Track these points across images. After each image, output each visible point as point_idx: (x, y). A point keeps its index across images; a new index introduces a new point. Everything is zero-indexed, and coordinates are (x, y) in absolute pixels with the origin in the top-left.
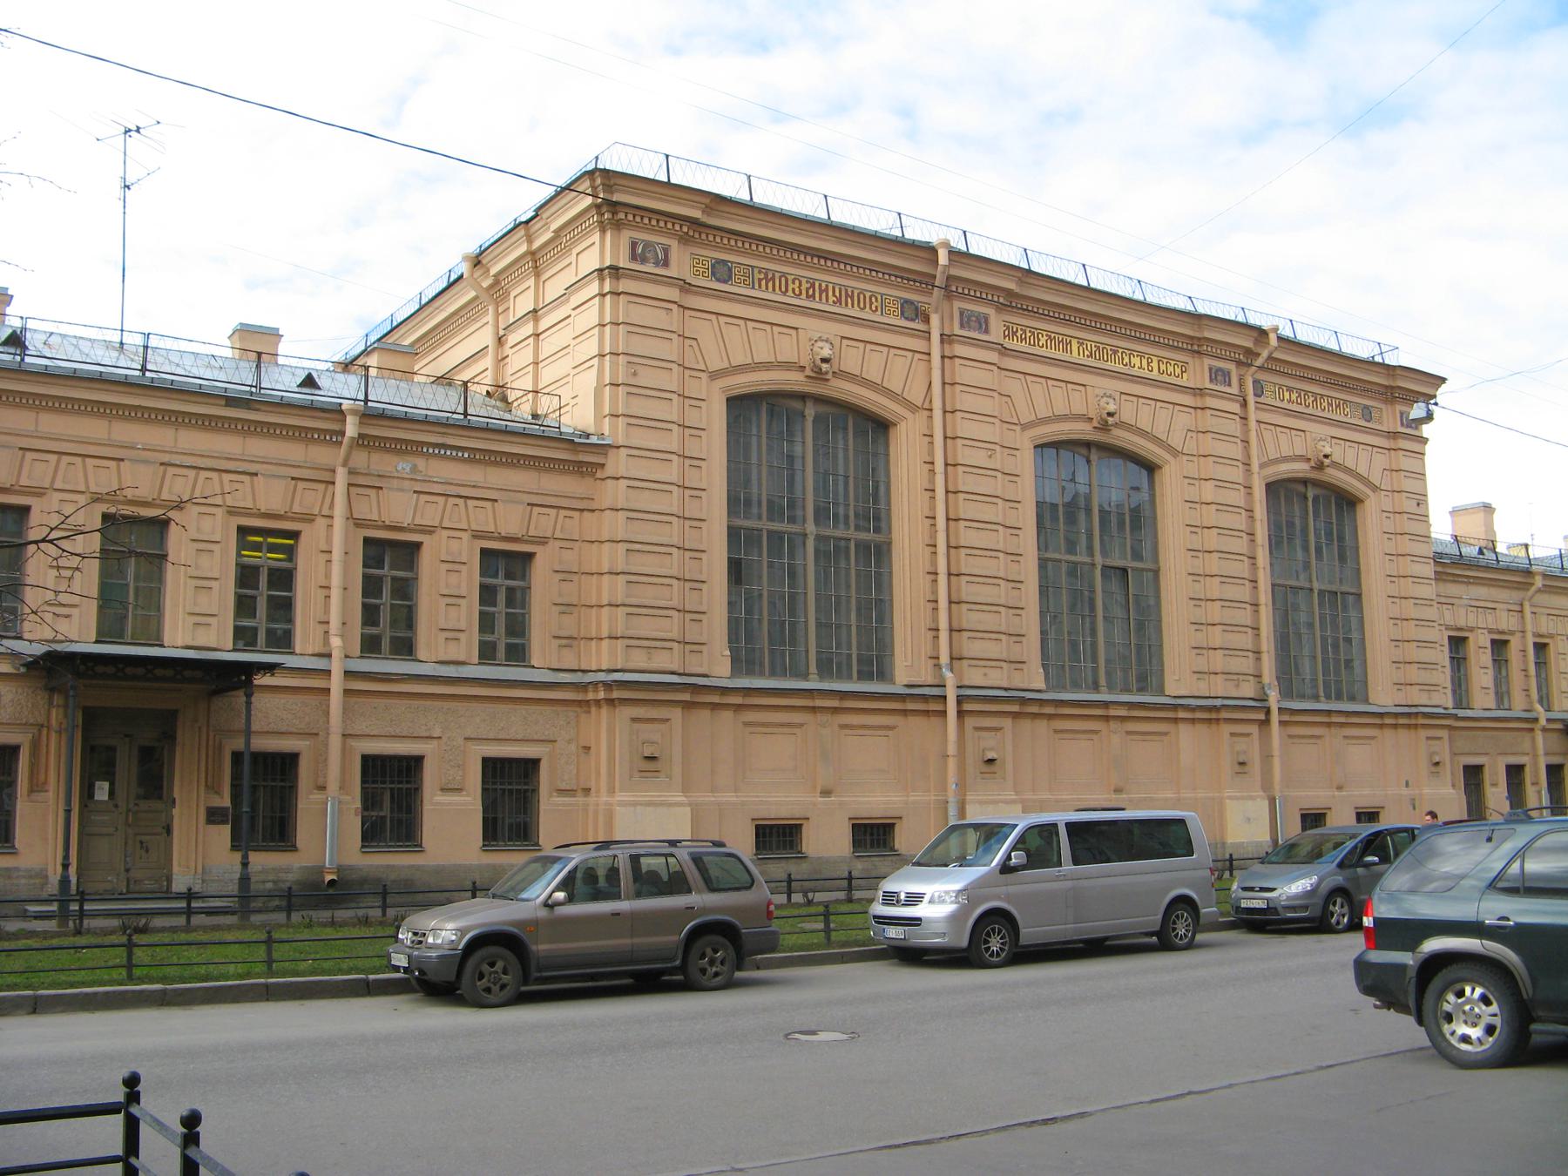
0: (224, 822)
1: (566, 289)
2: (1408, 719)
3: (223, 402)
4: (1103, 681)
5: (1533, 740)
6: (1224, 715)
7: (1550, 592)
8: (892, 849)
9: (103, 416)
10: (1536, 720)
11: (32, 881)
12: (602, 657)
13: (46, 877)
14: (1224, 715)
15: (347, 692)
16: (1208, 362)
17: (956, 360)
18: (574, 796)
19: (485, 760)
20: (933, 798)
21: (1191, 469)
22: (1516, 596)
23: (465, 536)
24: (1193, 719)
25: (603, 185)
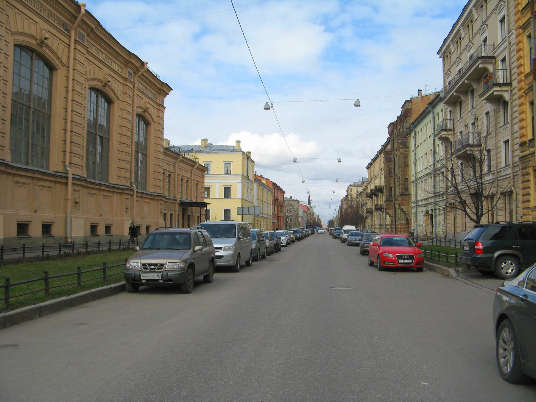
4: (30, 162)
5: (175, 206)
6: (126, 192)
8: (50, 235)
10: (176, 200)
14: (126, 192)
16: (129, 70)
20: (62, 215)
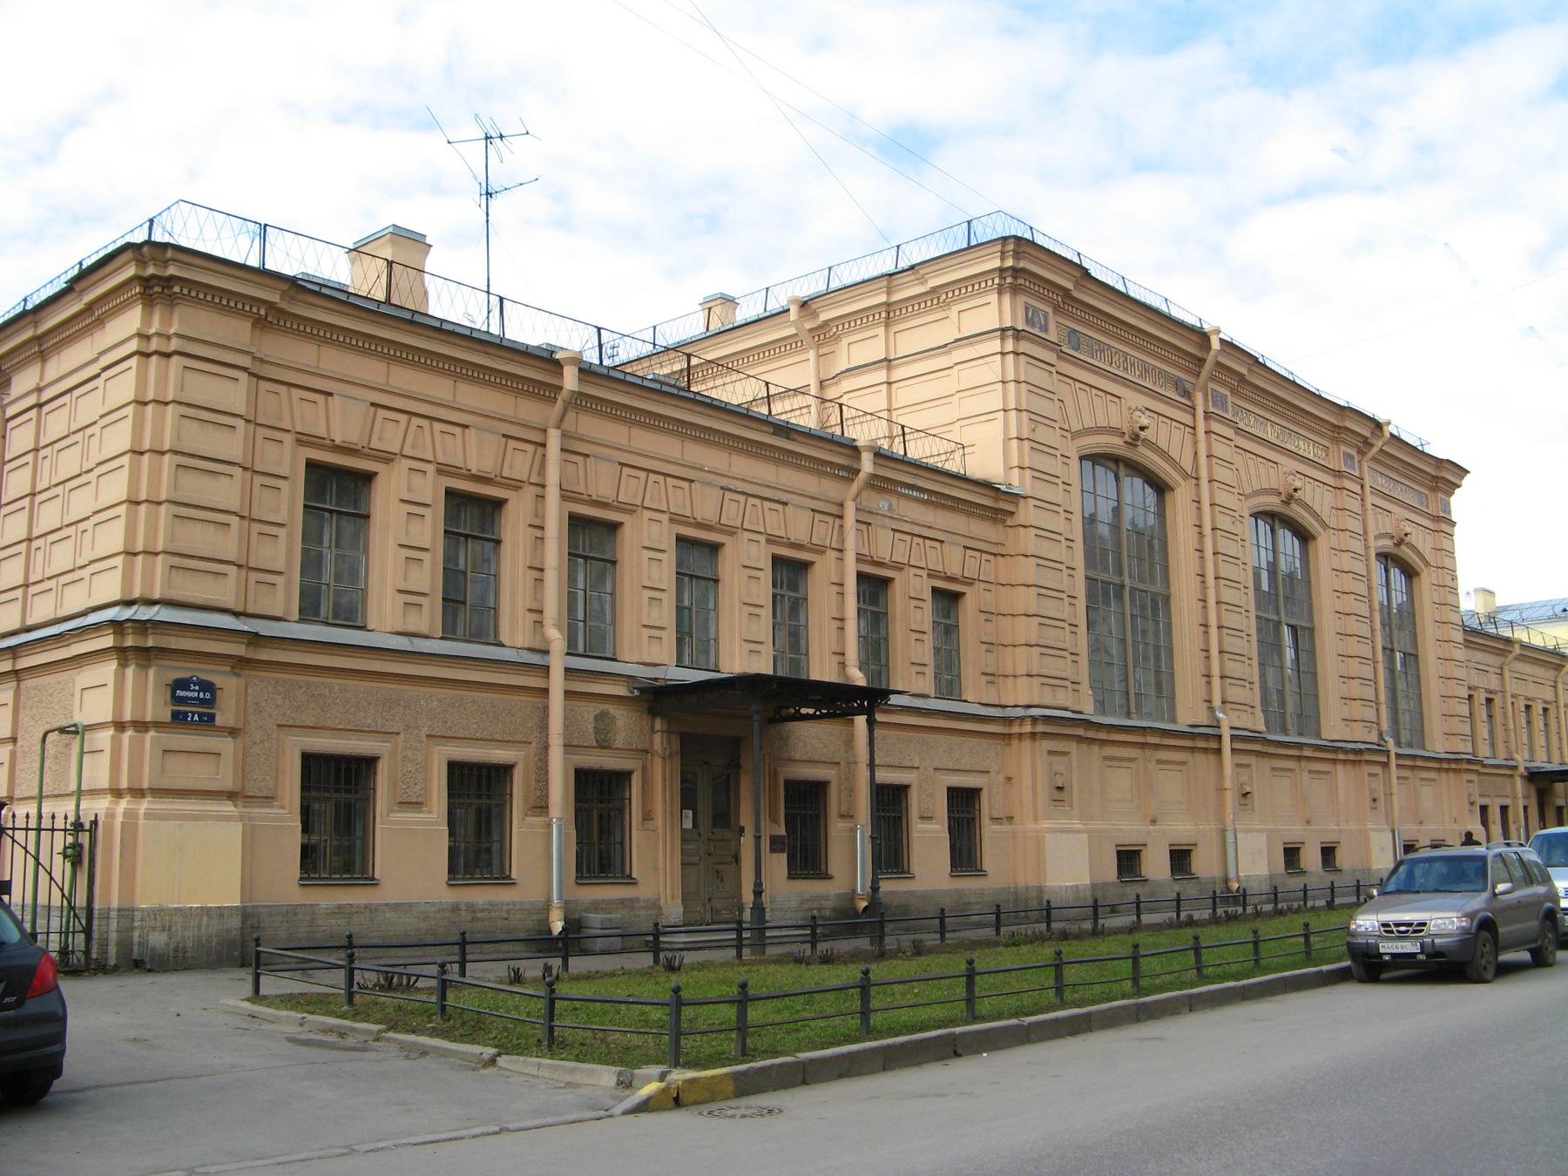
0: (782, 851)
1: (1147, 409)
2: (1452, 764)
3: (771, 430)
7: (1524, 661)
9: (677, 434)
10: (1515, 767)
11: (649, 912)
12: (1020, 693)
13: (660, 908)
15: (569, 694)
16: (1343, 448)
17: (1212, 435)
18: (1001, 824)
19: (950, 790)
21: (1334, 542)
22: (1499, 660)
23: (288, 439)
24: (1193, 748)
25: (1013, 251)
